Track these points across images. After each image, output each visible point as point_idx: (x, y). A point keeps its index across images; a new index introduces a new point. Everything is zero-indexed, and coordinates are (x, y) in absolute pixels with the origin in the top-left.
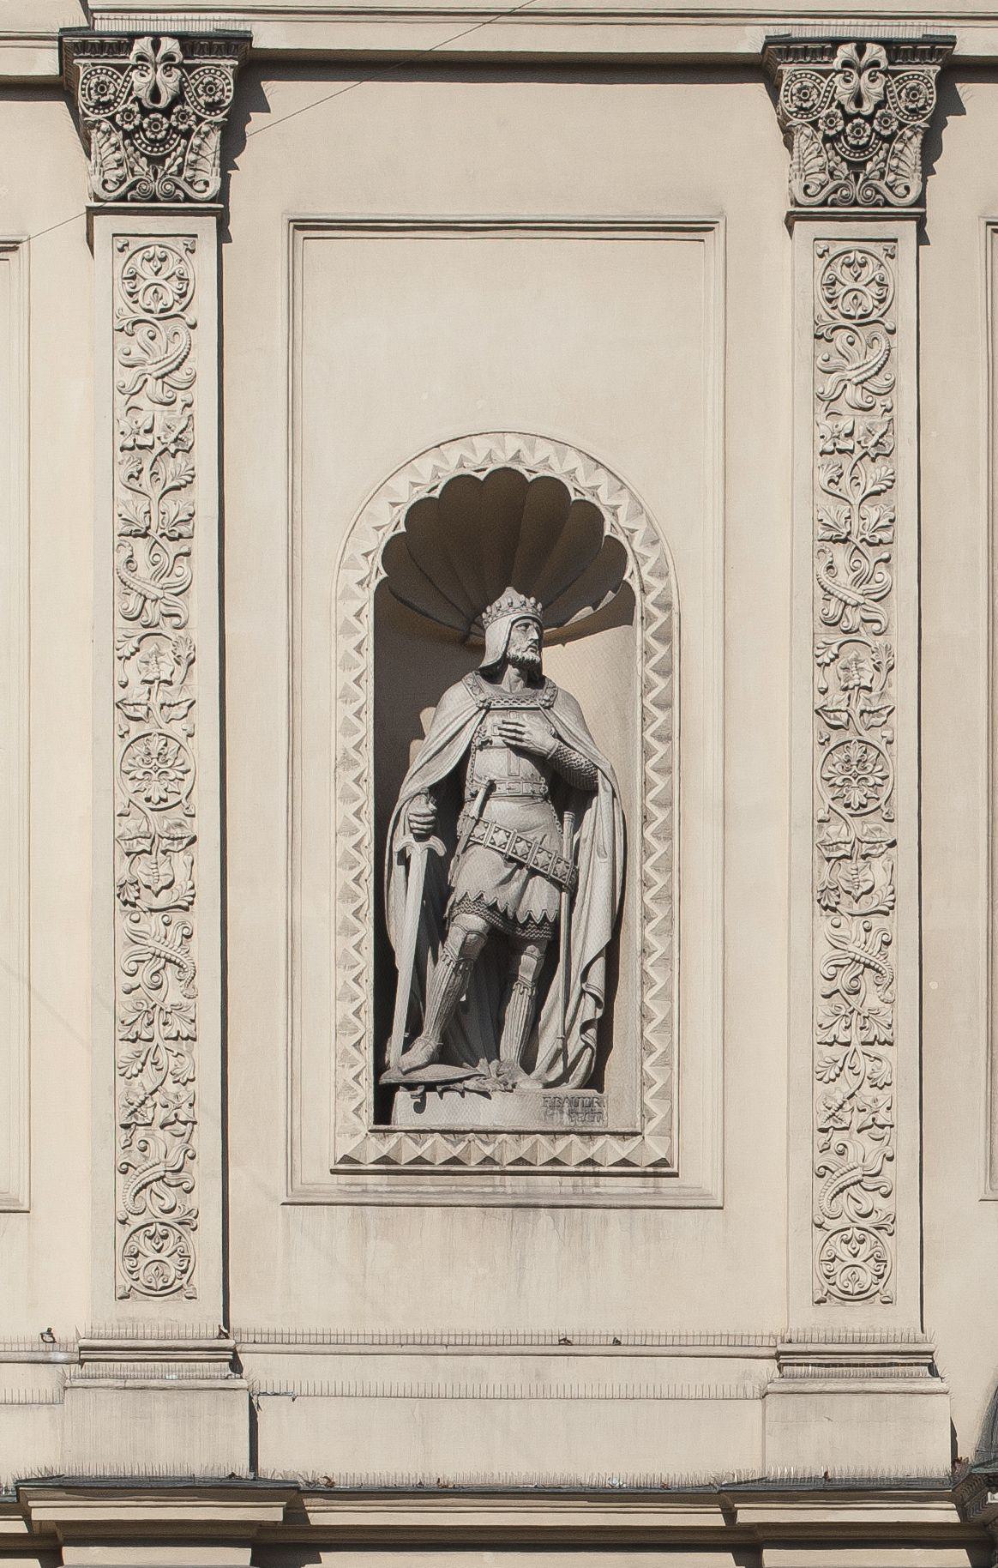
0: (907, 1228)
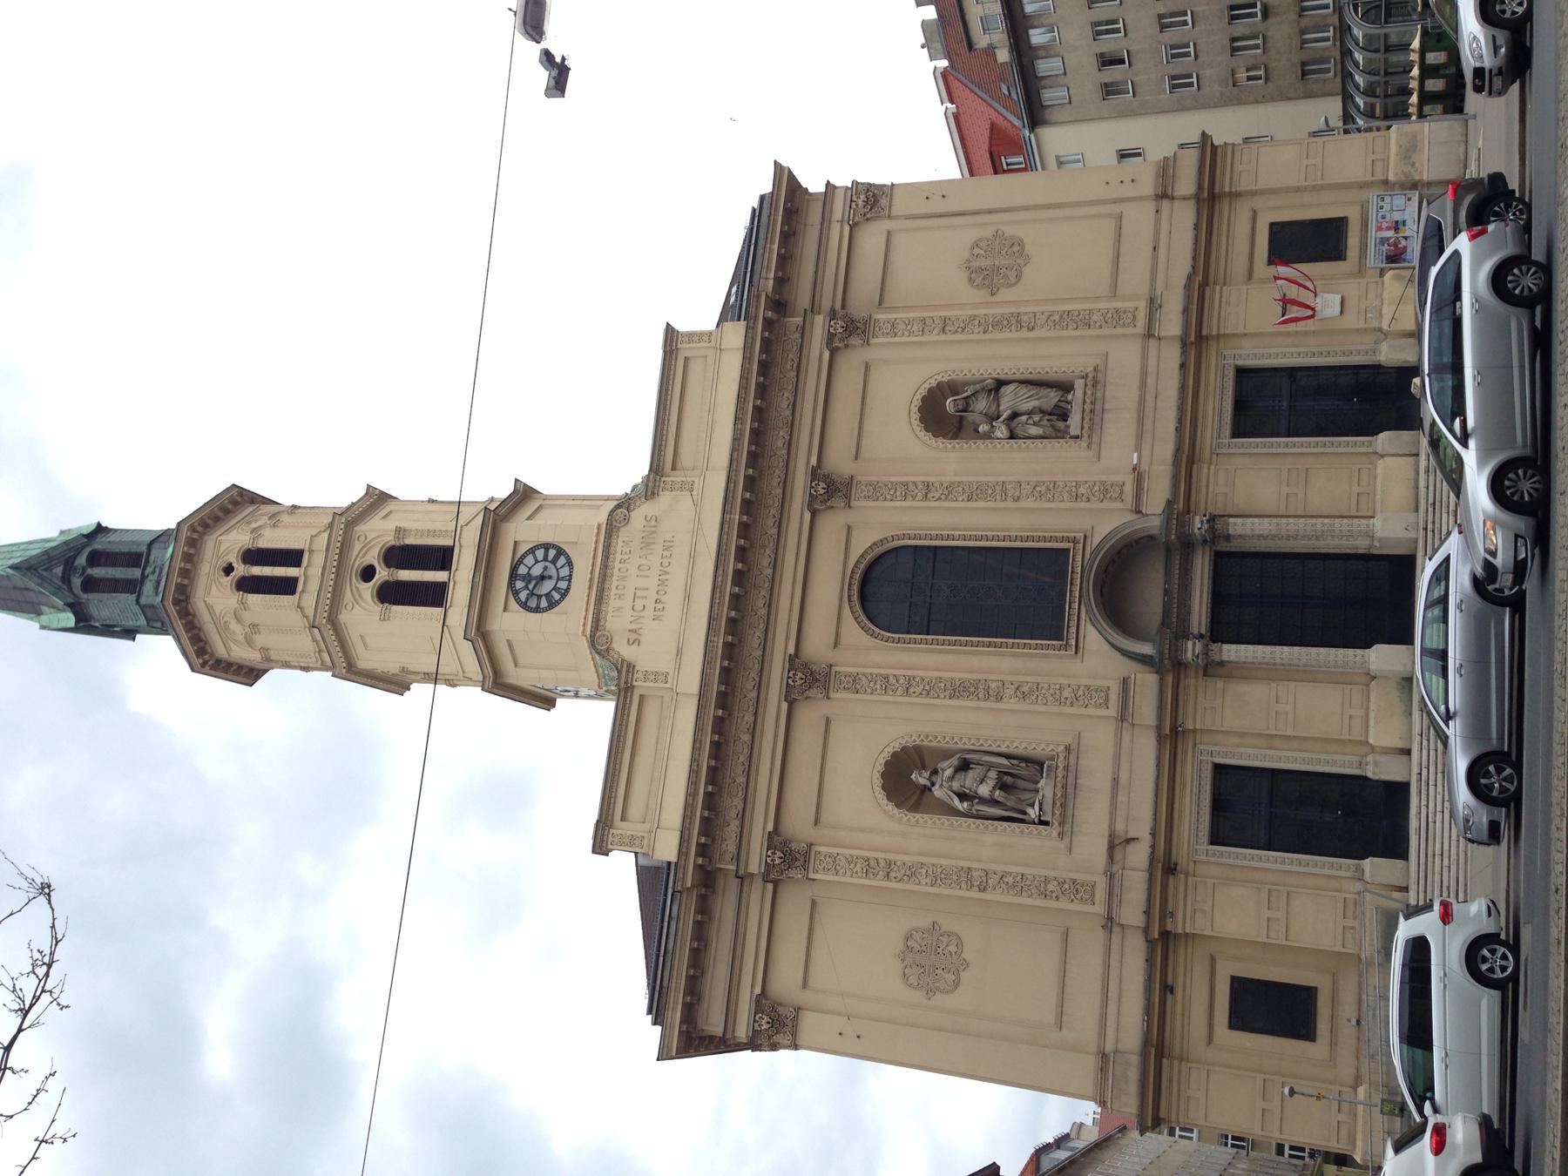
0: (1089, 682)
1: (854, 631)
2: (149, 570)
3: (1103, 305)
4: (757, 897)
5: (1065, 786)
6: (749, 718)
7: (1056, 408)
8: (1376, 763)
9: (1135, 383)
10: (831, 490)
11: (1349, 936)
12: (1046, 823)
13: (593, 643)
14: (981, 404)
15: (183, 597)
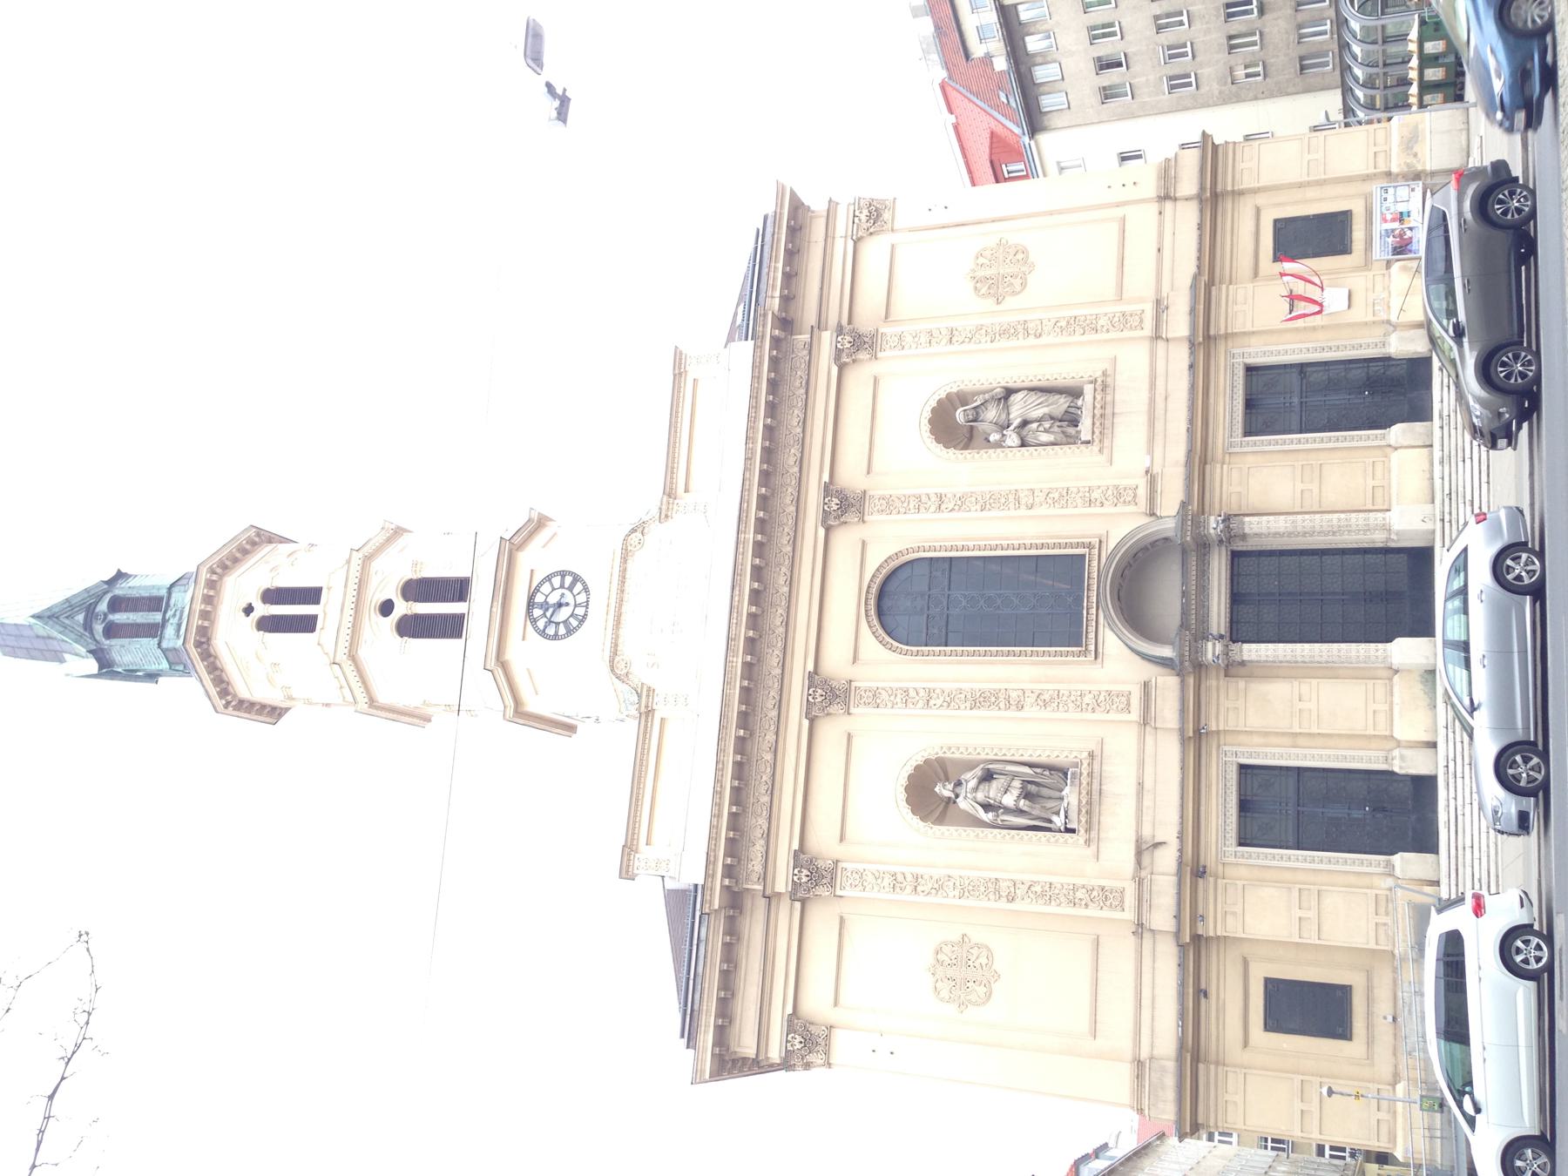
1: (872, 646)
2: (169, 613)
4: (786, 916)
5: (1090, 793)
6: (771, 737)
7: (1067, 414)
9: (1146, 386)
10: (844, 506)
12: (1073, 831)
15: (204, 639)
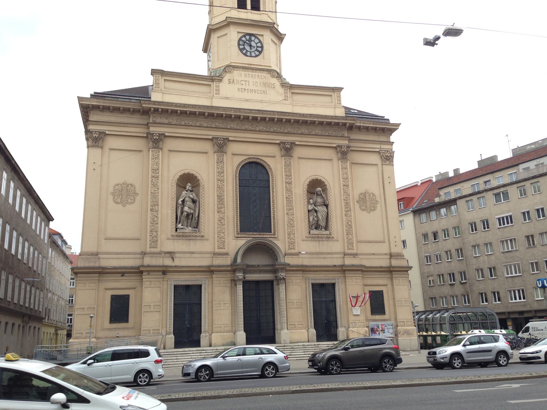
1: (238, 160)
3: (354, 239)
5: (190, 236)
7: (319, 225)
8: (206, 336)
10: (287, 150)
11: (147, 332)
12: (176, 231)
13: (228, 66)
14: (319, 200)
